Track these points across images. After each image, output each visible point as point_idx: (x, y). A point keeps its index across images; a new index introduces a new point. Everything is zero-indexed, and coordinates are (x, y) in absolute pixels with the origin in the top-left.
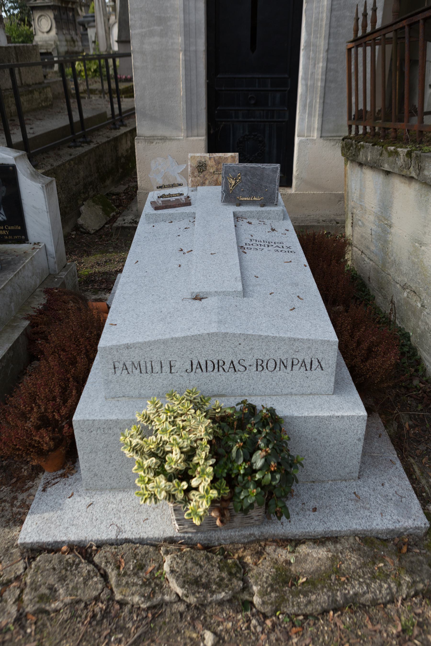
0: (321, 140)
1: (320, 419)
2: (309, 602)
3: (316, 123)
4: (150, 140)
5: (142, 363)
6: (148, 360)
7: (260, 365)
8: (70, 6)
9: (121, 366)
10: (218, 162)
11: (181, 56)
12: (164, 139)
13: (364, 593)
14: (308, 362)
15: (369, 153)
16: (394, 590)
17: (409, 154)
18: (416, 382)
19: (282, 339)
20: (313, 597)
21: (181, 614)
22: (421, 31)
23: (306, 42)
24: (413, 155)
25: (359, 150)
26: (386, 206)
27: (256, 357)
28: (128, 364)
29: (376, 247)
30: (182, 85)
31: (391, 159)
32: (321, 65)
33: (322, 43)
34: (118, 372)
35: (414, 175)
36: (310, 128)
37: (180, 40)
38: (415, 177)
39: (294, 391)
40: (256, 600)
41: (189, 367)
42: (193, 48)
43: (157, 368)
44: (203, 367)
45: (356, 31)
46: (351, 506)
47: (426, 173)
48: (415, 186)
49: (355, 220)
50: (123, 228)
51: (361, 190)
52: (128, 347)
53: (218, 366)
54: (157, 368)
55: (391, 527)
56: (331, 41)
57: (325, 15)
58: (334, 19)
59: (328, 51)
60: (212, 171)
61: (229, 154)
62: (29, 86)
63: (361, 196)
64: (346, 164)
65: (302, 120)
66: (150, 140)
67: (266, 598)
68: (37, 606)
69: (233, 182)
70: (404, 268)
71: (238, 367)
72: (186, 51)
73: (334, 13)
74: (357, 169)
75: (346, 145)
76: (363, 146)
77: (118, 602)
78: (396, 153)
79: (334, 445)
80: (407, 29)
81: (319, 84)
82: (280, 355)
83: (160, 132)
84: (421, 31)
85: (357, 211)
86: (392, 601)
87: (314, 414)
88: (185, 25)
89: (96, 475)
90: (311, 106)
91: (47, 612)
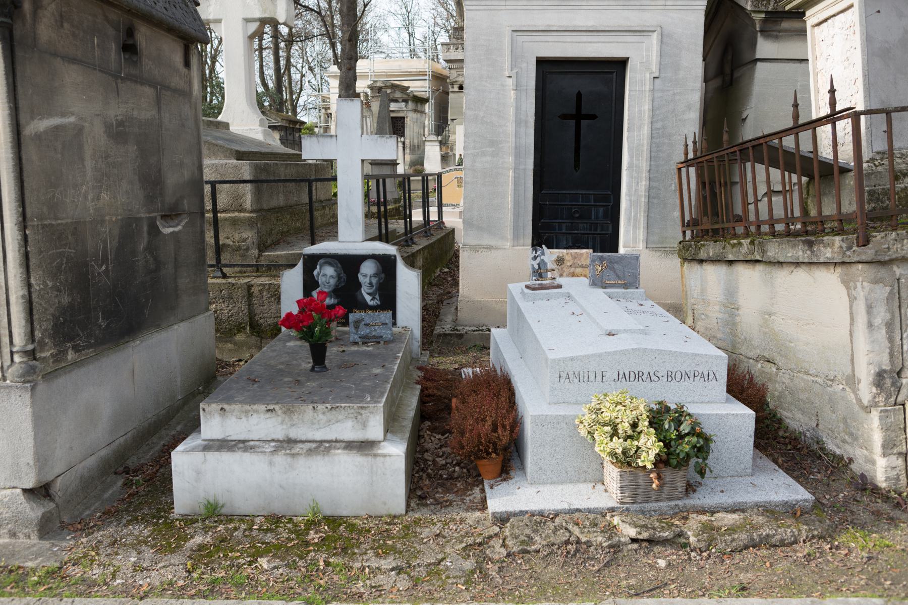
0: (647, 251)
1: (720, 417)
2: (733, 540)
3: (641, 234)
4: (476, 248)
5: (581, 373)
6: (586, 371)
7: (670, 376)
8: (297, 126)
9: (565, 375)
10: (574, 257)
11: (511, 173)
12: (489, 248)
13: (774, 535)
14: (706, 374)
15: (711, 249)
16: (796, 533)
17: (752, 243)
18: (781, 433)
19: (687, 354)
20: (736, 536)
21: (636, 551)
22: (751, 154)
23: (867, 128)
24: (756, 242)
25: (700, 248)
26: (731, 293)
27: (668, 369)
28: (571, 374)
29: (723, 333)
30: (510, 199)
31: (735, 250)
32: (644, 183)
33: (644, 165)
34: (562, 380)
35: (758, 258)
36: (635, 240)
37: (511, 159)
38: (760, 259)
39: (695, 399)
40: (692, 539)
41: (616, 377)
42: (522, 167)
43: (592, 378)
44: (627, 377)
45: (686, 154)
46: (750, 489)
47: (769, 254)
48: (759, 268)
49: (696, 315)
50: (445, 335)
51: (702, 285)
52: (572, 359)
53: (639, 376)
54: (592, 378)
55: (786, 499)
56: (652, 163)
57: (646, 142)
58: (653, 145)
59: (649, 171)
60: (569, 264)
61: (584, 251)
62: (321, 201)
63: (703, 291)
64: (682, 266)
65: (627, 231)
66: (476, 248)
67: (700, 537)
68: (521, 547)
69: (600, 269)
70: (755, 343)
71: (653, 378)
72: (516, 169)
73: (654, 140)
74: (696, 267)
75: (684, 247)
76: (704, 245)
77: (585, 543)
78: (740, 244)
79: (731, 441)
80: (738, 153)
81: (643, 199)
82: (685, 368)
83: (486, 241)
84: (751, 154)
85: (699, 308)
86: (795, 542)
87: (715, 412)
88: (516, 148)
89: (541, 469)
90: (635, 220)
91: (528, 552)
